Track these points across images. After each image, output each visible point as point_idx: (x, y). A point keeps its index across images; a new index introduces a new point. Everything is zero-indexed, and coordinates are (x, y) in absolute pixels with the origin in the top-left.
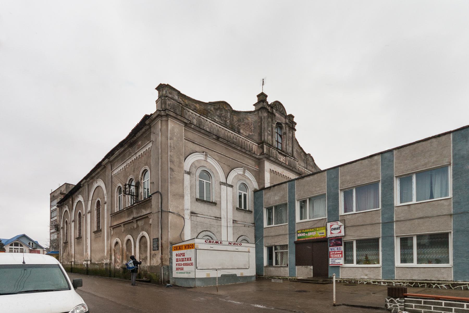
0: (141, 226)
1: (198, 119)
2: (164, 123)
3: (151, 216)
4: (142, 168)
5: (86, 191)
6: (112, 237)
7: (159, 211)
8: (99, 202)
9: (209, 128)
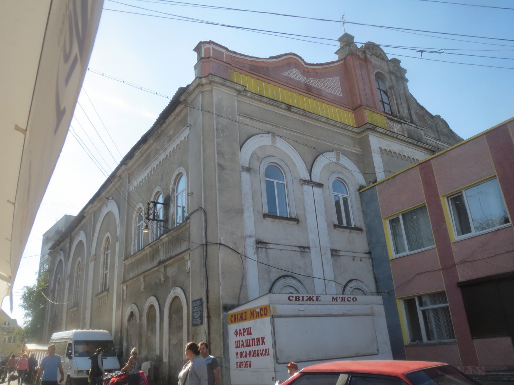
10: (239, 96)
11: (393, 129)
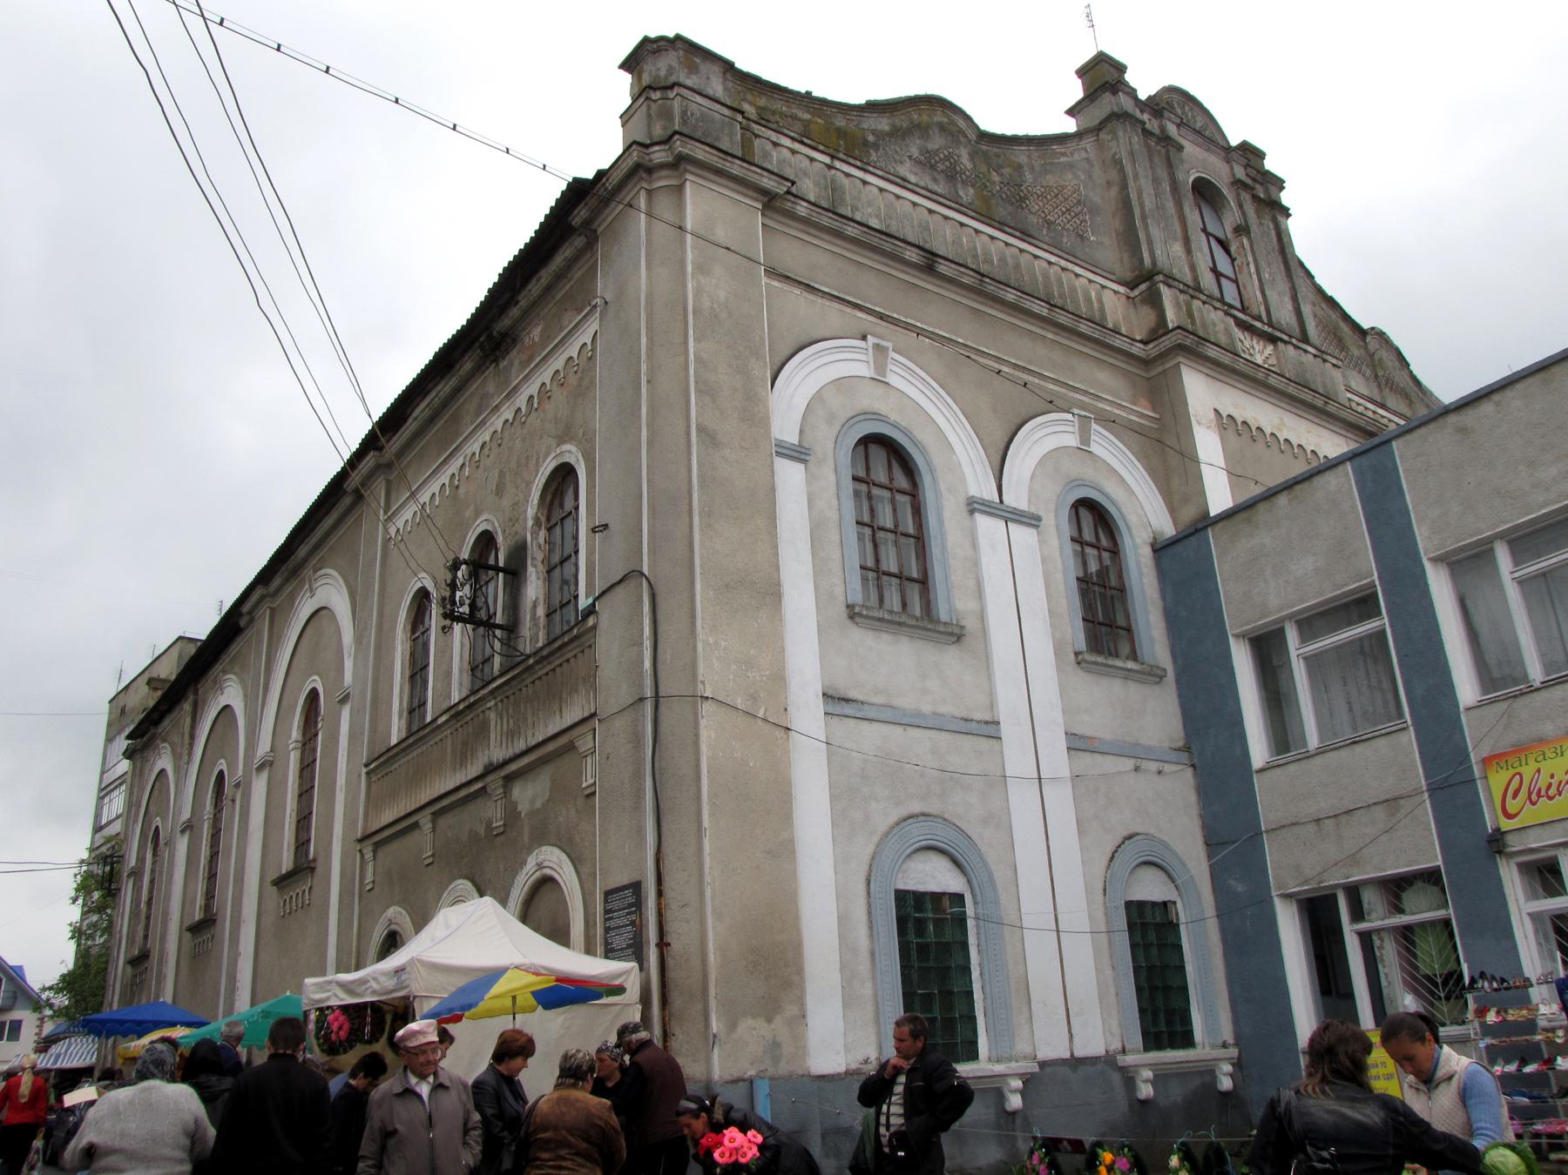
0: (533, 813)
1: (825, 178)
2: (664, 205)
3: (590, 737)
4: (544, 461)
5: (260, 641)
6: (1223, 213)
7: (642, 699)
8: (314, 694)
9: (878, 216)
10: (768, 213)
11: (1251, 355)
